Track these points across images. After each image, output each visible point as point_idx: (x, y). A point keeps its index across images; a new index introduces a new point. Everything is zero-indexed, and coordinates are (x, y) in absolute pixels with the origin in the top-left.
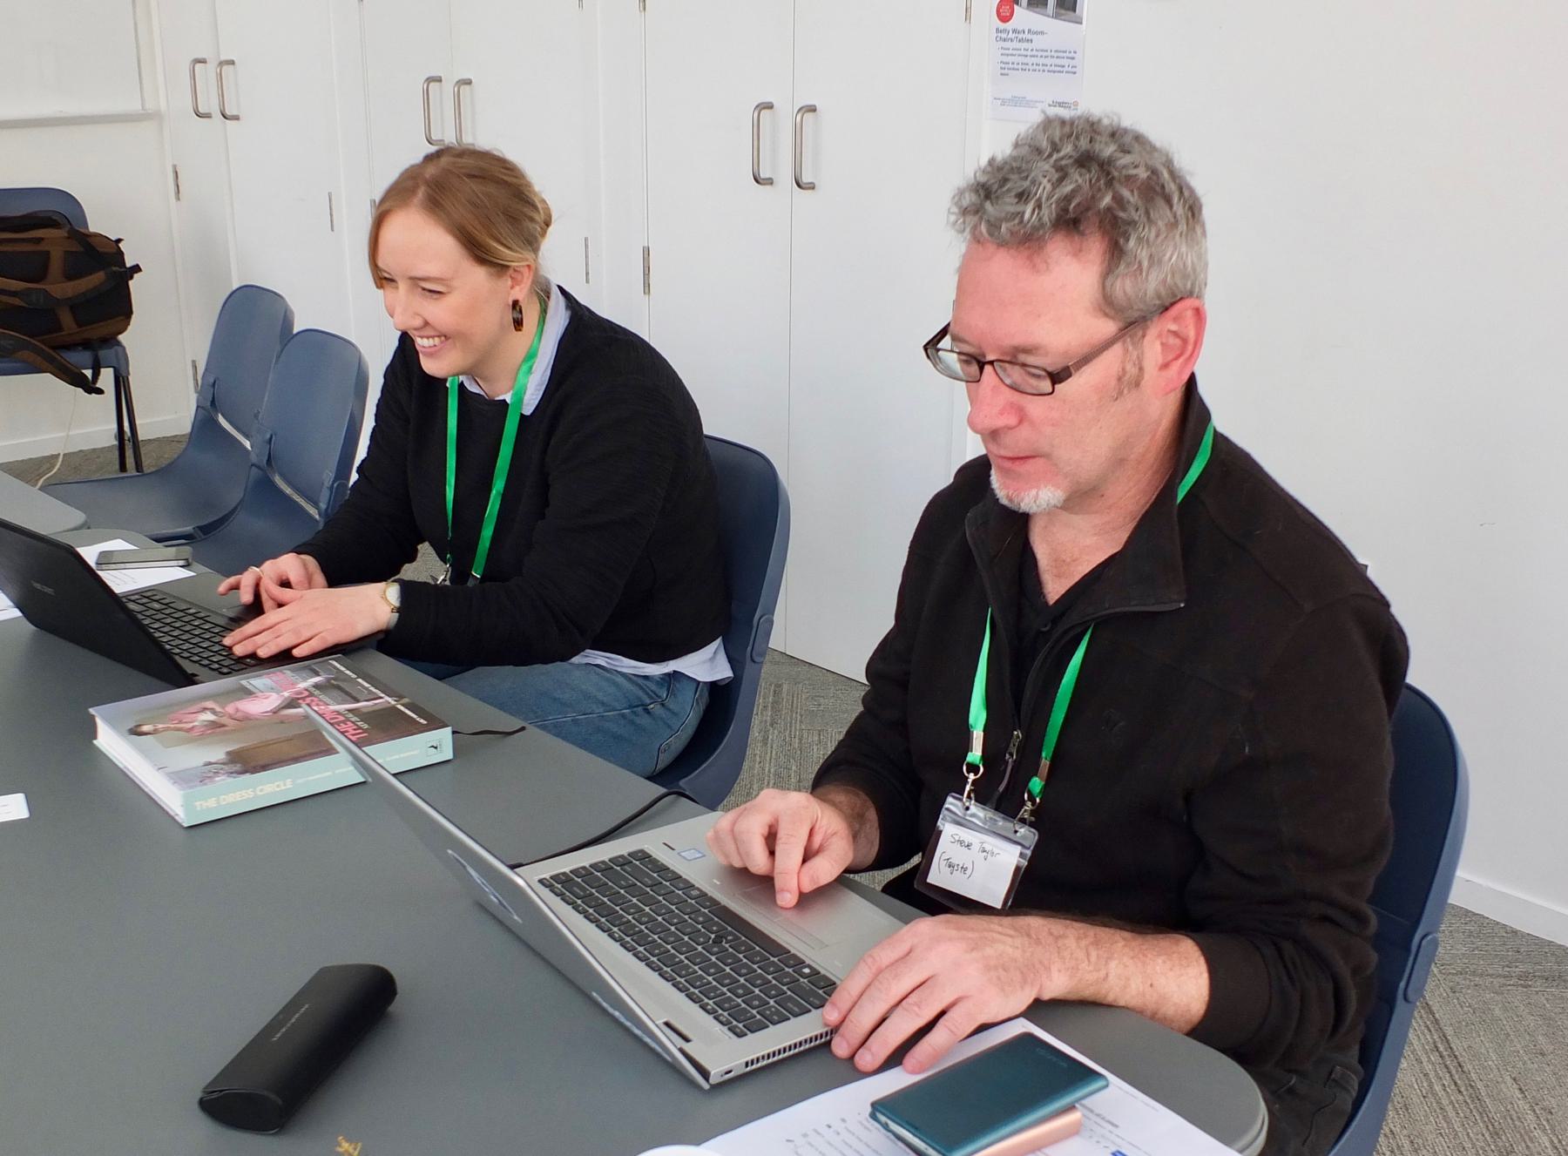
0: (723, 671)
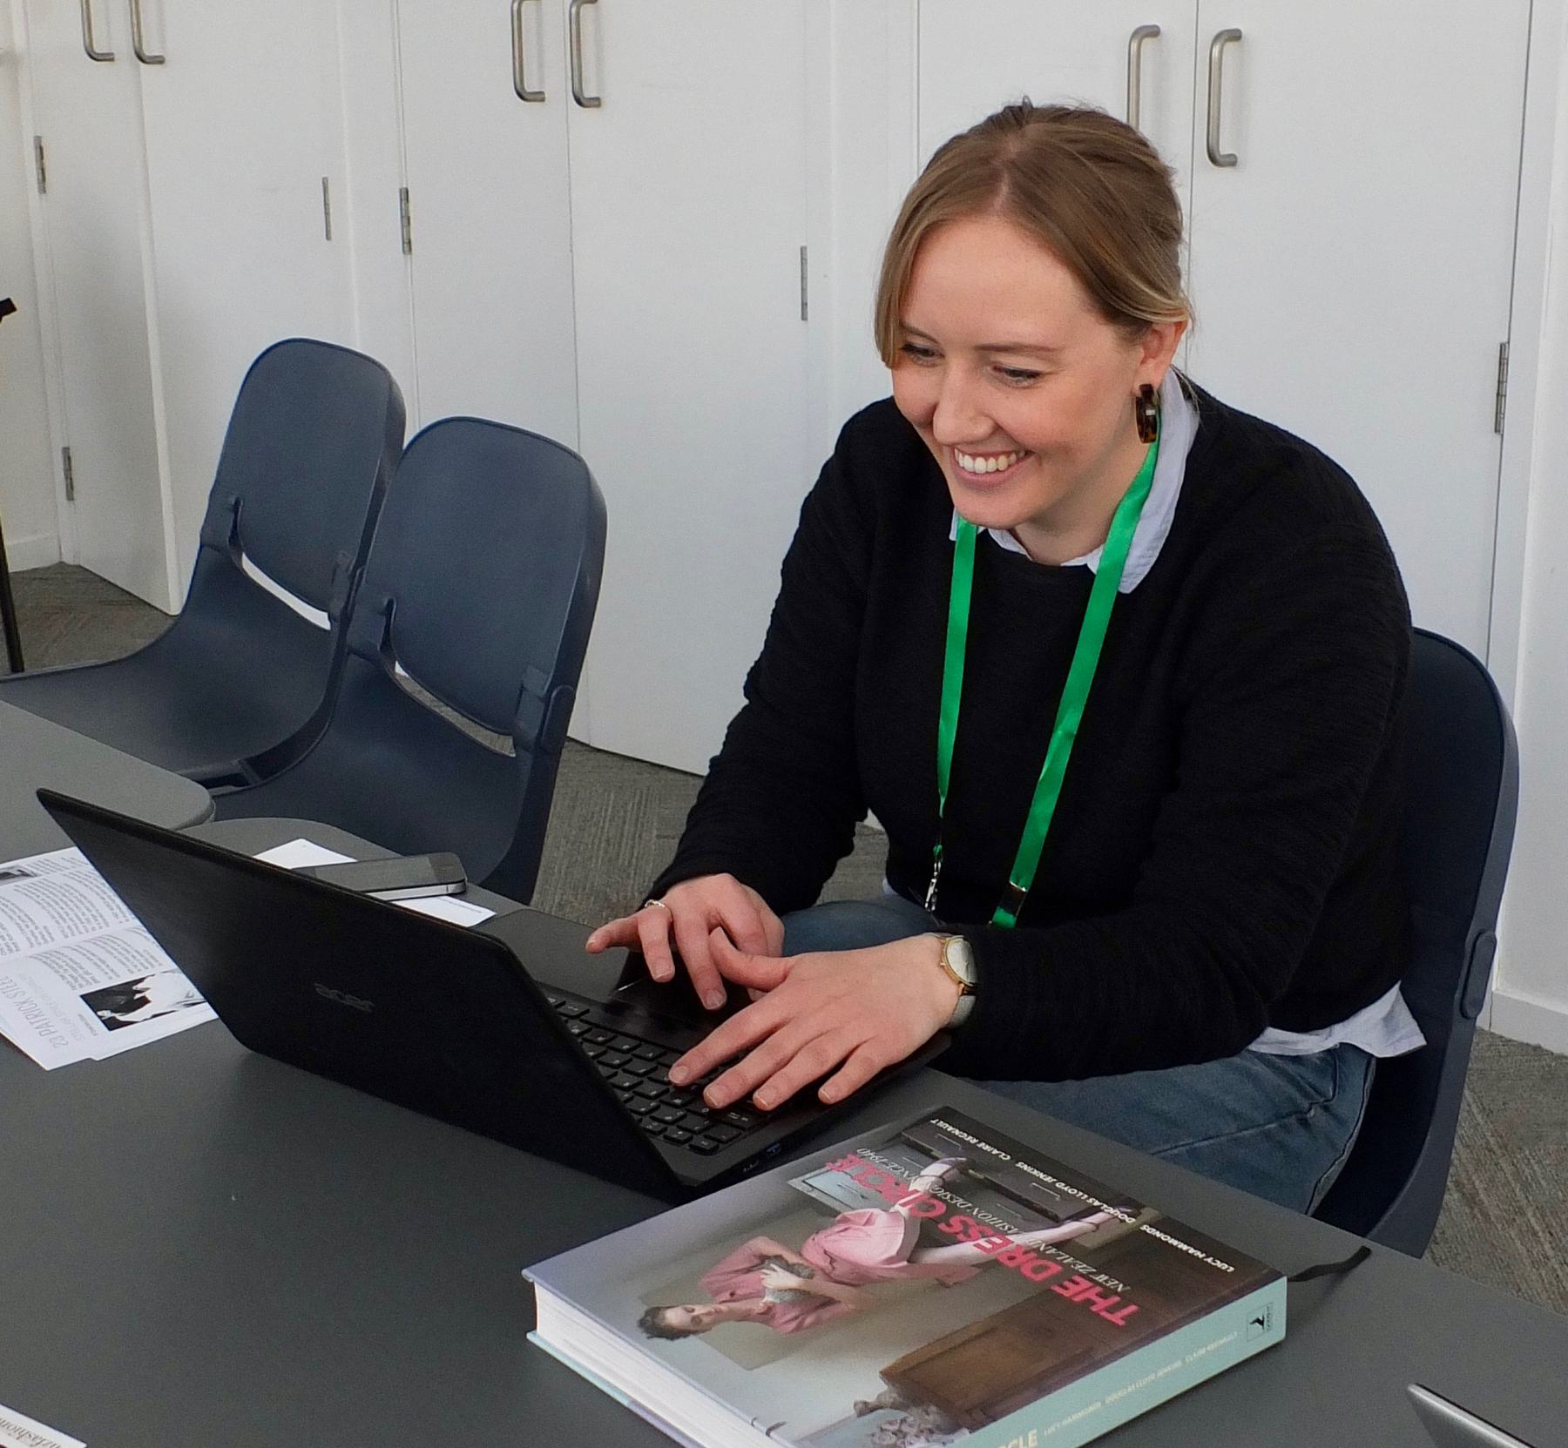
0: (1410, 1038)
